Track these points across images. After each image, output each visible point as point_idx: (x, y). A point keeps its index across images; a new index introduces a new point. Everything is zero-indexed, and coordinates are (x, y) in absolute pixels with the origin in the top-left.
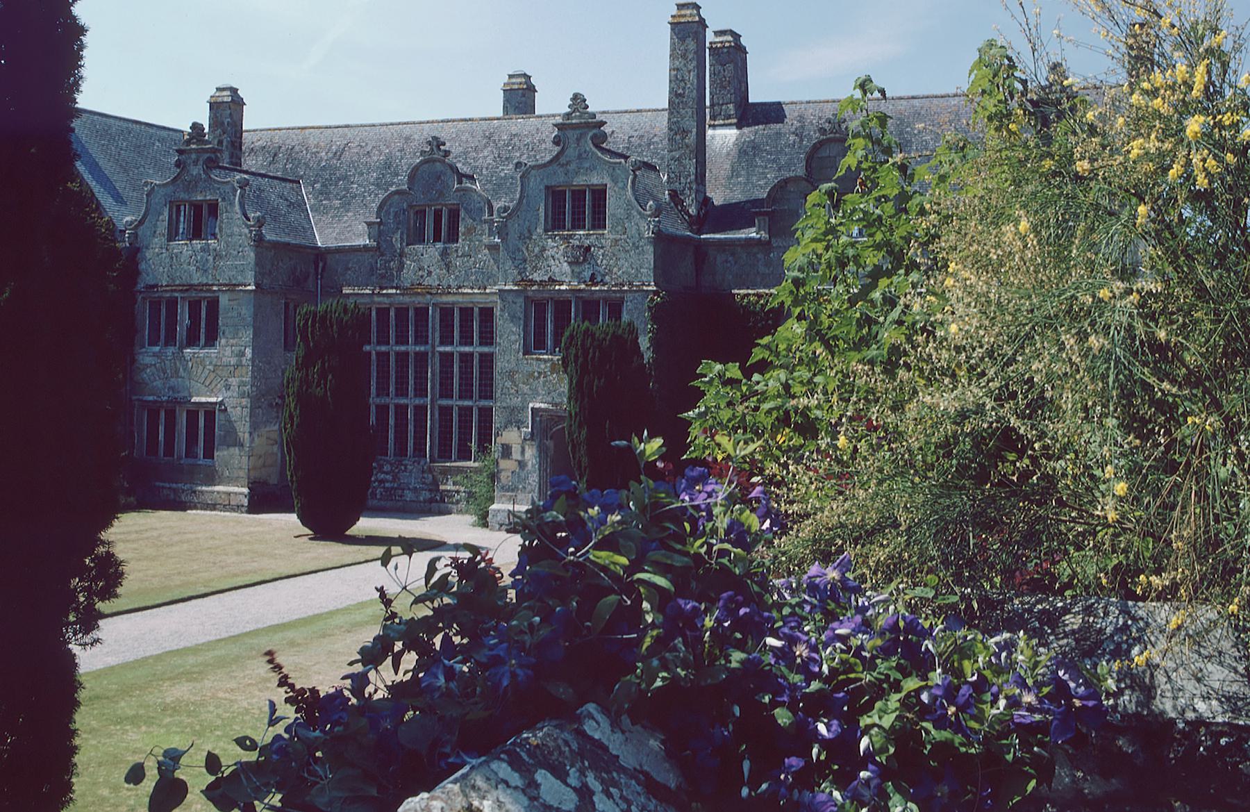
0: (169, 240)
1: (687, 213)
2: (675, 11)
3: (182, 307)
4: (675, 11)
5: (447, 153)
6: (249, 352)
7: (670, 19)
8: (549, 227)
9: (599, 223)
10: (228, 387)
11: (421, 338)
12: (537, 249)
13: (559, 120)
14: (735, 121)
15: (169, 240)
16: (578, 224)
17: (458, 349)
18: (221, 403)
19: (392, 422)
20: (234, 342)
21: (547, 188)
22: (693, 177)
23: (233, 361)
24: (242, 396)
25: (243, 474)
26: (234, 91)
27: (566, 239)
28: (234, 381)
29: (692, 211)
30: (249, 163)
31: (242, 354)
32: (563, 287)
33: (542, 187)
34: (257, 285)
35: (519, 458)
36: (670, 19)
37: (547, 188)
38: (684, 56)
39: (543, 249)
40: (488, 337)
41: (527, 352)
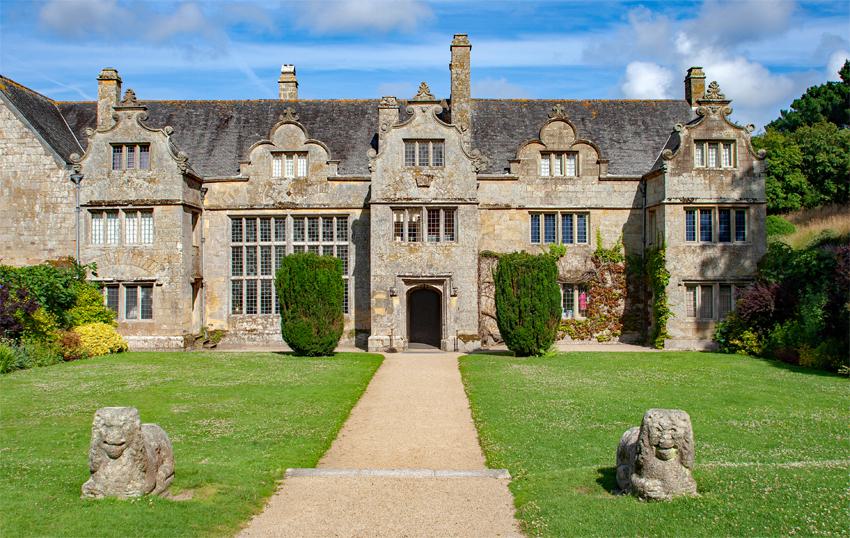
11: (280, 235)
16: (424, 162)
17: (244, 244)
19: (259, 292)
27: (417, 171)
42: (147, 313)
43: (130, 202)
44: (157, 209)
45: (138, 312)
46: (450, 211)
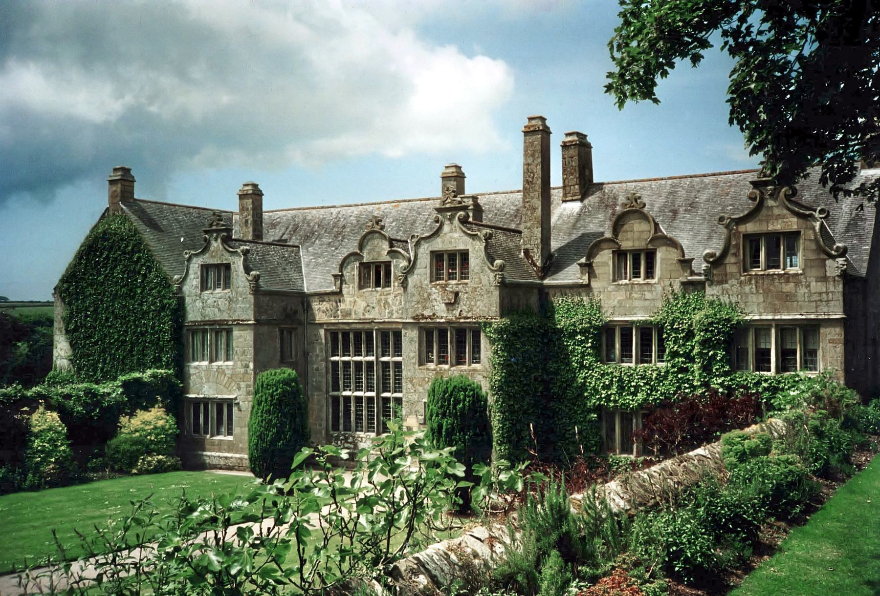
0: (202, 290)
1: (535, 265)
2: (526, 123)
3: (211, 336)
4: (526, 123)
5: (382, 228)
6: (251, 365)
7: (523, 129)
8: (434, 279)
9: (465, 275)
10: (239, 388)
12: (426, 295)
13: (754, 177)
14: (579, 197)
15: (202, 290)
16: (451, 277)
18: (236, 399)
20: (243, 358)
21: (432, 252)
22: (539, 241)
23: (242, 371)
24: (248, 393)
25: (247, 445)
26: (255, 186)
27: (444, 287)
28: (243, 385)
29: (539, 264)
30: (271, 236)
31: (247, 366)
32: (443, 320)
33: (428, 252)
34: (256, 320)
35: (232, 520)
36: (523, 129)
37: (432, 252)
38: (533, 155)
39: (430, 294)
40: (398, 351)
41: (420, 364)
43: (214, 322)
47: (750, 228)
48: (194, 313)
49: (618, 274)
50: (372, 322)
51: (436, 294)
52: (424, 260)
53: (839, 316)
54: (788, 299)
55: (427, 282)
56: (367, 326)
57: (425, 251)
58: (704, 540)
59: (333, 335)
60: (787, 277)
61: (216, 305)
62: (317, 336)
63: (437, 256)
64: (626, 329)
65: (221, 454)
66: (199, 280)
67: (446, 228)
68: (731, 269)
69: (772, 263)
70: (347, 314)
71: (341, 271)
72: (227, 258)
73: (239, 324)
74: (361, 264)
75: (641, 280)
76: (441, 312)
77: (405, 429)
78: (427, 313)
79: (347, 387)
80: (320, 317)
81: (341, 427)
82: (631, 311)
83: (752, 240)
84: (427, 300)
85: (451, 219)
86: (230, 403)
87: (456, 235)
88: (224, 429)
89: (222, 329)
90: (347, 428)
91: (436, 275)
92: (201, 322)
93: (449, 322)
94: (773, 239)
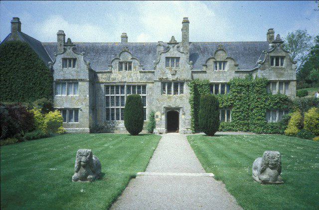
27: (171, 69)
42: (76, 120)
43: (70, 80)
44: (80, 83)
45: (73, 120)
46: (182, 84)
47: (272, 54)
48: (57, 76)
49: (121, 69)
50: (125, 82)
51: (168, 71)
52: (163, 59)
53: (295, 79)
54: (282, 74)
55: (164, 67)
56: (122, 84)
57: (163, 56)
58: (298, 98)
59: (107, 87)
60: (282, 69)
61: (70, 73)
62: (100, 88)
63: (167, 58)
64: (217, 85)
65: (73, 129)
66: (61, 64)
67: (171, 50)
68: (267, 66)
69: (277, 64)
70: (114, 79)
71: (206, 63)
72: (75, 56)
73: (81, 80)
74: (119, 62)
75: (222, 70)
76: (170, 78)
77: (155, 116)
78: (164, 78)
79: (113, 105)
80: (101, 80)
81: (110, 119)
82: (220, 80)
83: (272, 58)
84: (164, 73)
85: (173, 47)
86: (77, 110)
87: (176, 52)
88: (73, 120)
89: (74, 82)
90: (113, 119)
91: (167, 65)
92: (63, 80)
93: (173, 80)
94: (277, 58)
